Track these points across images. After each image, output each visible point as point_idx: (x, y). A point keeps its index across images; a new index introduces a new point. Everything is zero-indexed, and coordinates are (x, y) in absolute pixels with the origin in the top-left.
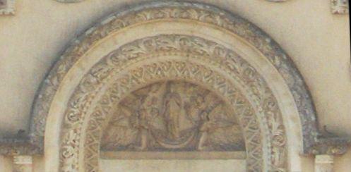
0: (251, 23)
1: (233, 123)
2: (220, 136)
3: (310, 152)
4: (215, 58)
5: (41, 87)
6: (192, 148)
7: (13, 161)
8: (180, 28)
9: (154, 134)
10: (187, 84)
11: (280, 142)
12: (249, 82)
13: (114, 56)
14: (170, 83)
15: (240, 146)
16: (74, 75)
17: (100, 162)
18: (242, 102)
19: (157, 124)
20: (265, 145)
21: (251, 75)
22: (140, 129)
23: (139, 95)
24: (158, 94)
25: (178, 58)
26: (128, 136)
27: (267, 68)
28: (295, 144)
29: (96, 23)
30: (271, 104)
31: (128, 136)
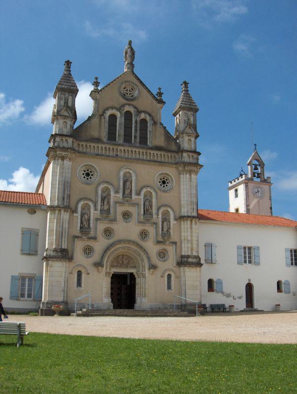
0: (140, 245)
1: (134, 263)
2: (131, 265)
3: (149, 269)
4: (133, 251)
5: (106, 251)
6: (127, 267)
7: (188, 311)
8: (128, 245)
9: (120, 264)
10: (126, 255)
11: (144, 267)
12: (139, 256)
13: (116, 250)
14: (123, 255)
15: (135, 267)
16: (109, 253)
17: (255, 308)
18: (137, 259)
19: (121, 262)
20: (141, 267)
21: (139, 255)
22: (118, 263)
23: (118, 257)
24: (121, 257)
25: (127, 251)
26: (116, 264)
27: (142, 254)
28: (147, 267)
29: (113, 244)
30: (142, 260)
31: (116, 264)
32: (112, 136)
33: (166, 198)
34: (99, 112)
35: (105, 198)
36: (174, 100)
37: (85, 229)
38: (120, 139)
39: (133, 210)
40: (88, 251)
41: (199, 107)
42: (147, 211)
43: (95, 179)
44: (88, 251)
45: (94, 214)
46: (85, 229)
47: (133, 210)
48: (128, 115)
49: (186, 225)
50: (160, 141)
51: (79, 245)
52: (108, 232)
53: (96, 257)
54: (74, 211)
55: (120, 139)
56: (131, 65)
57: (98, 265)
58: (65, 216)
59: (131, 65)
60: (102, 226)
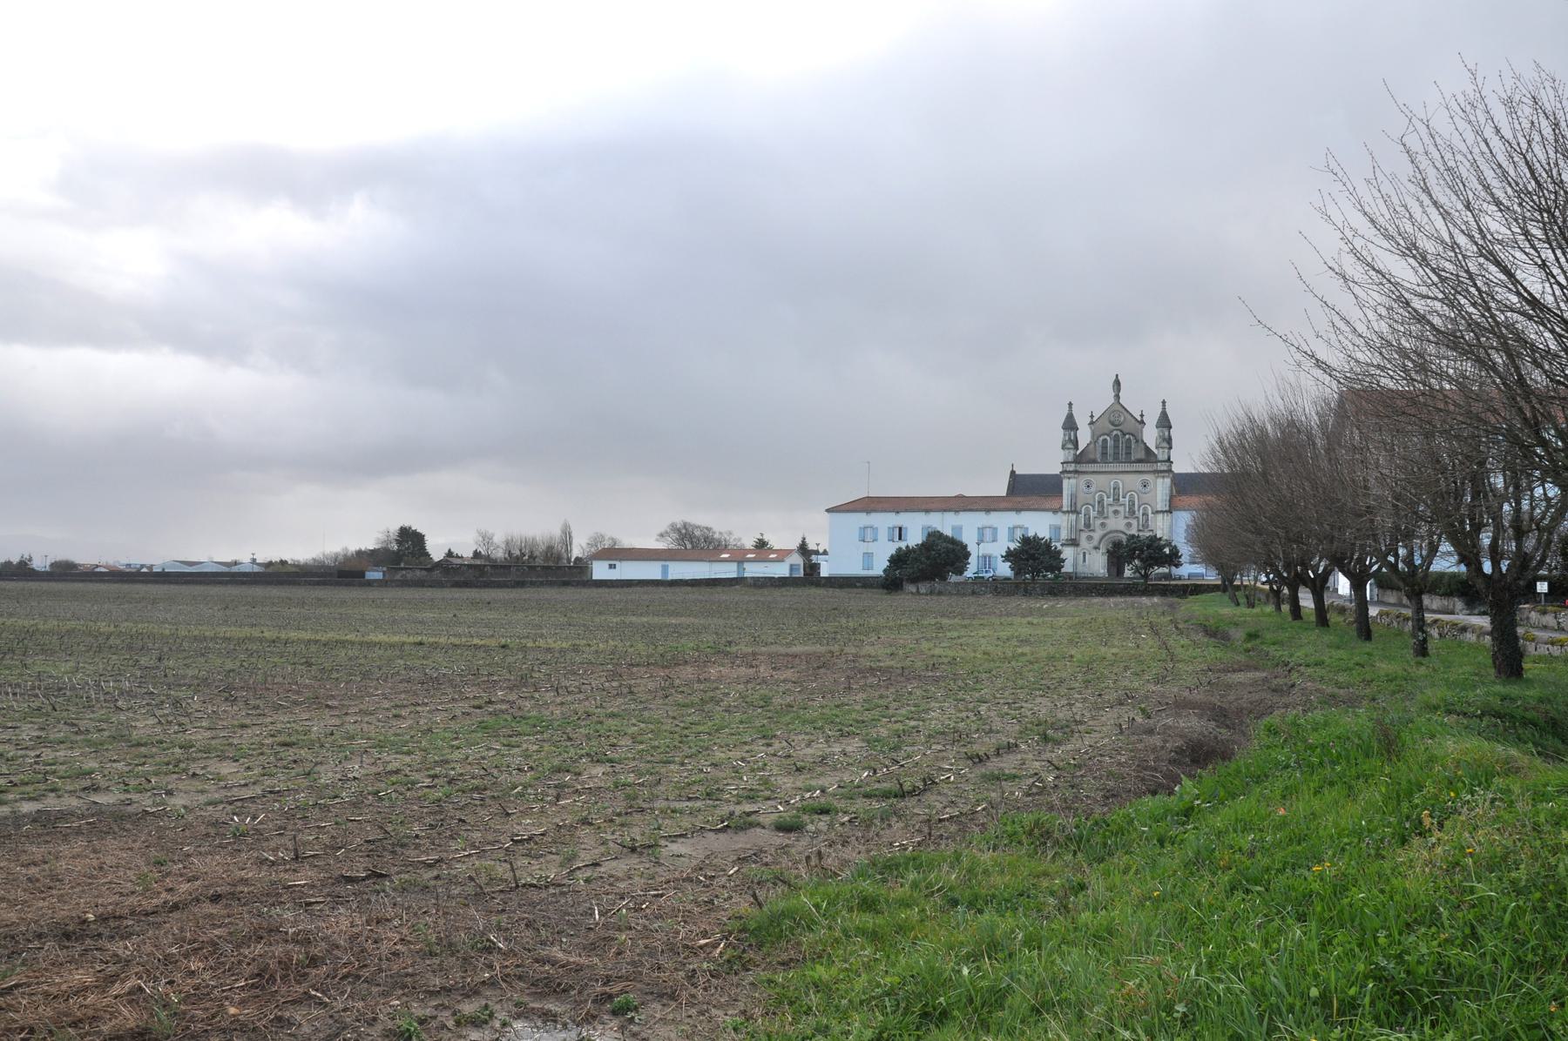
11: (1168, 576)
32: (1104, 454)
33: (1146, 498)
34: (1094, 441)
35: (1101, 502)
36: (1151, 420)
37: (1087, 525)
38: (1123, 457)
39: (1121, 509)
40: (1090, 538)
41: (394, 528)
42: (1132, 512)
43: (1093, 489)
44: (1090, 538)
45: (1093, 514)
46: (1087, 525)
47: (1121, 509)
48: (1116, 439)
49: (1160, 516)
50: (1141, 455)
51: (1084, 536)
52: (1103, 525)
53: (1095, 543)
54: (1078, 513)
55: (1123, 457)
56: (1117, 397)
57: (1096, 548)
58: (1073, 517)
59: (1117, 397)
60: (1098, 522)
